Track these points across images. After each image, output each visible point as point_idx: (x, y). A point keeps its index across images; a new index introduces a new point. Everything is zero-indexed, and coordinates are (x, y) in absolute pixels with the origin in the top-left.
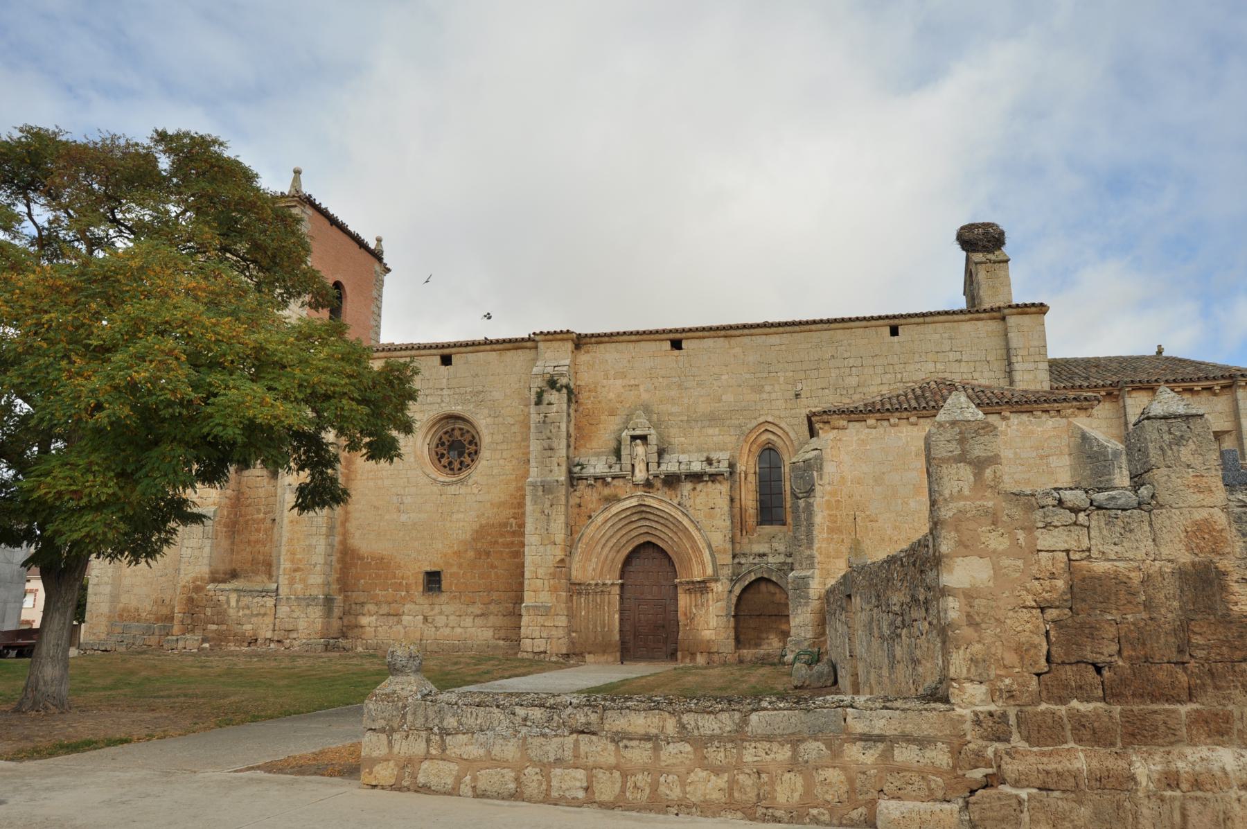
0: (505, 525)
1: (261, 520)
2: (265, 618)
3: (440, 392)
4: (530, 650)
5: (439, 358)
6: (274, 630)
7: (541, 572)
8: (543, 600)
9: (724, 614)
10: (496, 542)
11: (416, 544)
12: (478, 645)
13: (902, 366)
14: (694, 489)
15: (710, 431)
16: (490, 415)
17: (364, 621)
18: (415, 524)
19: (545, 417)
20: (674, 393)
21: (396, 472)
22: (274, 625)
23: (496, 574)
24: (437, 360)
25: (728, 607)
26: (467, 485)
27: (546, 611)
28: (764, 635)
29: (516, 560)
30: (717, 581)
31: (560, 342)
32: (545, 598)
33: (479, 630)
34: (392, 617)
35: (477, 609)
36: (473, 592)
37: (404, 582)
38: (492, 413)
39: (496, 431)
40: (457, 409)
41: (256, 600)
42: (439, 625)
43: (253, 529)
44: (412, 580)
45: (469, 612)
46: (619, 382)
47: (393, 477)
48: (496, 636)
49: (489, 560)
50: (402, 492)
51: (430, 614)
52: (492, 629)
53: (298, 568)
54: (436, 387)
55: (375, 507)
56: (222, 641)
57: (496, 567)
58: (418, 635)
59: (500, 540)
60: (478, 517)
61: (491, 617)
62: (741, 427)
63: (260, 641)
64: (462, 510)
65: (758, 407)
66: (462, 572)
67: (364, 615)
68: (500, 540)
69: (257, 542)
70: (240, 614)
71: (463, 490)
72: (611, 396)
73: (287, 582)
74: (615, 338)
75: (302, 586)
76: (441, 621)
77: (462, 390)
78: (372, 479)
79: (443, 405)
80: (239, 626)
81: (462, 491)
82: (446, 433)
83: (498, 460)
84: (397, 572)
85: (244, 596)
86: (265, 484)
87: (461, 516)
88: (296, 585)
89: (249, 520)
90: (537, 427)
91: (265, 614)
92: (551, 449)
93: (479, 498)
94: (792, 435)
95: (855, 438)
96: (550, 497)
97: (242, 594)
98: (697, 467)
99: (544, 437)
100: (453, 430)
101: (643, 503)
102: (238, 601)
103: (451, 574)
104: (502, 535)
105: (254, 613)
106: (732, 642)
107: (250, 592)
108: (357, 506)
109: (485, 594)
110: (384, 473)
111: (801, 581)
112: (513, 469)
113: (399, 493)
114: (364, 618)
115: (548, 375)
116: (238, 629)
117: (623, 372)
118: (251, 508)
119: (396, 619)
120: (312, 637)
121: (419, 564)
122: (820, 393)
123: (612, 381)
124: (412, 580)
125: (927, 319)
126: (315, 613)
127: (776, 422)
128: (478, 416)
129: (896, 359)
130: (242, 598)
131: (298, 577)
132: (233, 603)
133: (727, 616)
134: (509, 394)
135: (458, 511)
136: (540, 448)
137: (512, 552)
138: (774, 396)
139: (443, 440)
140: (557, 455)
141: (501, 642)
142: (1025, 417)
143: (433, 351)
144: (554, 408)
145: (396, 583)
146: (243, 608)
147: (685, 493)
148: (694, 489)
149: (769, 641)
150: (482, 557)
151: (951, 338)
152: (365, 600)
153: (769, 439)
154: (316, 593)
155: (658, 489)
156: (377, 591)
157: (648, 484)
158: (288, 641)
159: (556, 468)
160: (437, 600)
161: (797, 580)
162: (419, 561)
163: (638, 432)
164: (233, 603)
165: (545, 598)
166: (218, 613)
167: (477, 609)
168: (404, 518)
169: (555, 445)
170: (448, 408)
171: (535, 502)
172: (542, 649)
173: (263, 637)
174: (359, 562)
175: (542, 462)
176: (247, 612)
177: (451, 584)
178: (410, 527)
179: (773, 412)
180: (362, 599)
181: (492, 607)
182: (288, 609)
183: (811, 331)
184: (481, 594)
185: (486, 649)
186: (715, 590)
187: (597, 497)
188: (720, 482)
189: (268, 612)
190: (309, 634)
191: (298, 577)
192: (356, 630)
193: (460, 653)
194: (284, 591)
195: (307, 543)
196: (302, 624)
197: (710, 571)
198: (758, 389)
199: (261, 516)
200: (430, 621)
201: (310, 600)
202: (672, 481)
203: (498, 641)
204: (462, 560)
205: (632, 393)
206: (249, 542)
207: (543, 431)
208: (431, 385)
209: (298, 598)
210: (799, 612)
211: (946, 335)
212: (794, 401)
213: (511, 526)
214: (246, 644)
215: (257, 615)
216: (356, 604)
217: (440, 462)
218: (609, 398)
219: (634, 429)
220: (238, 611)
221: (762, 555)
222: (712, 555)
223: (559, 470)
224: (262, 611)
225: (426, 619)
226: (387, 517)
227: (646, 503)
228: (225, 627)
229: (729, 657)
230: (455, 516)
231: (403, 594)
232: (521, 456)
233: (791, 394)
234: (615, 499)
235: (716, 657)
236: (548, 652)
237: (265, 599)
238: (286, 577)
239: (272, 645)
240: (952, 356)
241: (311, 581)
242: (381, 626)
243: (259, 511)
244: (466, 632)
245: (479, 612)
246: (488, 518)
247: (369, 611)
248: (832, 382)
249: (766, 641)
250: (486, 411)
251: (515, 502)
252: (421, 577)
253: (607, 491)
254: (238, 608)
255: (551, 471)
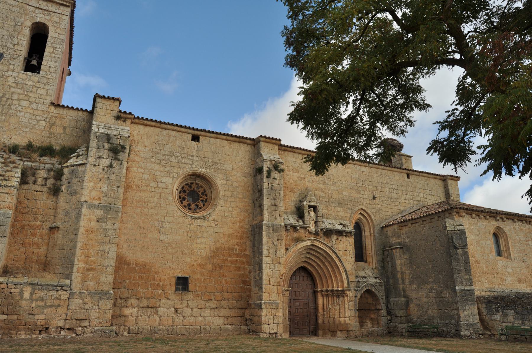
0: (232, 249)
1: (38, 227)
2: (58, 309)
3: (191, 158)
4: (268, 332)
5: (191, 136)
6: (66, 320)
7: (272, 280)
8: (274, 299)
9: (353, 309)
10: (226, 260)
11: (171, 256)
12: (214, 329)
13: (412, 192)
14: (338, 239)
15: (339, 209)
16: (224, 179)
17: (127, 311)
18: (171, 243)
19: (272, 186)
20: (322, 186)
21: (158, 205)
22: (67, 315)
23: (226, 280)
24: (190, 137)
25: (355, 305)
26: (208, 221)
27: (274, 306)
28: (364, 321)
29: (239, 272)
30: (350, 290)
31: (272, 145)
32: (275, 297)
33: (214, 318)
34: (150, 309)
35: (213, 304)
36: (210, 292)
37: (161, 284)
38: (225, 177)
39: (227, 188)
40: (203, 171)
41: (50, 293)
42: (186, 315)
43: (29, 233)
44: (167, 283)
45: (207, 305)
46: (295, 174)
47: (156, 208)
48: (226, 323)
49: (221, 271)
50: (163, 219)
51: (180, 307)
52: (223, 318)
53: (92, 268)
54: (189, 153)
55: (141, 227)
56: (10, 329)
57: (226, 276)
58: (170, 322)
59: (229, 259)
60: (215, 242)
61: (222, 310)
62: (352, 209)
63: (52, 329)
64: (204, 237)
65: (358, 201)
66: (203, 279)
67: (126, 307)
68: (229, 259)
69: (32, 244)
70: (34, 305)
71: (205, 224)
72: (291, 181)
73: (80, 279)
74: (295, 150)
75: (94, 283)
76: (187, 312)
77: (206, 160)
78: (139, 207)
79: (194, 166)
80: (31, 316)
81: (205, 224)
82: (187, 184)
83: (228, 207)
84: (156, 276)
85: (39, 289)
86: (44, 198)
87: (204, 240)
88: (89, 282)
89: (25, 225)
90: (267, 191)
91: (58, 306)
92: (276, 205)
93: (216, 230)
94: (373, 217)
95: (468, 222)
96: (277, 234)
97: (37, 287)
98: (339, 227)
99: (272, 198)
100: (192, 183)
101: (314, 244)
102: (31, 294)
103: (196, 280)
104: (230, 256)
105: (48, 304)
106: (358, 324)
107: (46, 287)
108: (126, 225)
109: (218, 294)
110: (150, 204)
111: (467, 292)
112: (238, 215)
113: (160, 220)
114: (127, 309)
115: (274, 162)
116: (29, 319)
117: (297, 170)
118: (28, 216)
119: (153, 310)
120: (103, 325)
121: (172, 271)
122: (383, 199)
123: (291, 173)
124: (167, 283)
125: (421, 174)
126: (106, 305)
127: (366, 209)
128: (216, 178)
129: (409, 190)
130: (36, 292)
131: (91, 275)
132: (27, 295)
133: (354, 310)
134: (235, 168)
135: (202, 237)
136: (269, 204)
137: (236, 267)
138: (365, 197)
139: (184, 189)
140: (279, 210)
141: (229, 327)
142: (520, 223)
143: (189, 131)
144: (277, 182)
145: (155, 283)
146: (37, 300)
147: (334, 241)
148: (338, 239)
149: (367, 324)
150: (217, 269)
151: (427, 184)
152: (129, 296)
153: (360, 218)
154: (107, 289)
155: (321, 237)
156: (140, 289)
157: (316, 234)
158: (80, 328)
159: (279, 217)
160: (185, 297)
161: (464, 291)
162: (173, 269)
163: (312, 204)
164: (27, 295)
165: (275, 297)
166: (10, 304)
167: (213, 304)
168: (163, 237)
169: (278, 203)
170: (197, 169)
171: (269, 236)
172: (275, 331)
173: (55, 325)
174: (126, 267)
175: (271, 213)
176: (41, 303)
177: (195, 286)
178: (167, 245)
179: (365, 204)
180: (126, 295)
181: (223, 303)
182: (81, 302)
183: (378, 168)
184: (216, 294)
185: (220, 332)
186: (349, 295)
187: (291, 238)
188: (349, 237)
189: (62, 304)
190: (101, 323)
191: (91, 275)
192: (120, 319)
193: (202, 335)
194: (76, 286)
195: (101, 249)
196: (94, 314)
197: (346, 285)
198: (359, 192)
199: (38, 223)
200: (179, 312)
201: (102, 295)
202: (328, 233)
203: (227, 326)
204: (203, 270)
205: (302, 181)
206: (23, 244)
207: (271, 194)
208: (185, 151)
209: (90, 293)
210: (467, 308)
211: (426, 182)
212: (373, 200)
213: (236, 250)
214: (37, 332)
215: (51, 306)
216: (121, 298)
217: (182, 203)
218: (291, 182)
219: (309, 202)
220: (31, 303)
221: (365, 277)
222: (347, 276)
223: (280, 219)
224: (56, 302)
225: (176, 311)
226: (150, 235)
227: (315, 244)
228: (15, 317)
229: (358, 333)
230: (199, 240)
231: (160, 292)
232: (242, 207)
233: (372, 197)
234: (298, 240)
235: (351, 333)
236: (279, 333)
237: (60, 292)
238: (79, 275)
239: (63, 333)
240: (429, 192)
241: (103, 279)
242: (141, 316)
243: (36, 219)
244: (205, 320)
245: (214, 306)
246: (222, 243)
247: (132, 304)
248: (387, 194)
249: (365, 324)
250: (221, 176)
251: (239, 235)
252: (174, 280)
253: (295, 235)
254: (31, 300)
255: (276, 219)
